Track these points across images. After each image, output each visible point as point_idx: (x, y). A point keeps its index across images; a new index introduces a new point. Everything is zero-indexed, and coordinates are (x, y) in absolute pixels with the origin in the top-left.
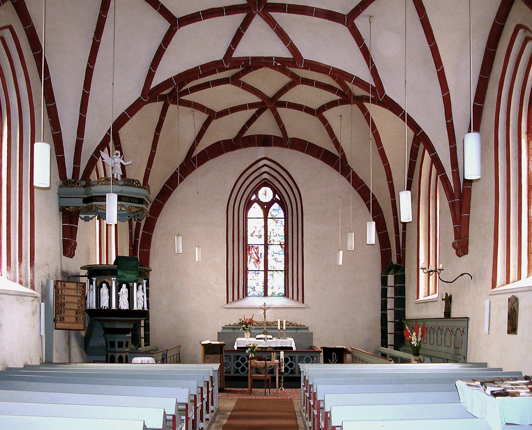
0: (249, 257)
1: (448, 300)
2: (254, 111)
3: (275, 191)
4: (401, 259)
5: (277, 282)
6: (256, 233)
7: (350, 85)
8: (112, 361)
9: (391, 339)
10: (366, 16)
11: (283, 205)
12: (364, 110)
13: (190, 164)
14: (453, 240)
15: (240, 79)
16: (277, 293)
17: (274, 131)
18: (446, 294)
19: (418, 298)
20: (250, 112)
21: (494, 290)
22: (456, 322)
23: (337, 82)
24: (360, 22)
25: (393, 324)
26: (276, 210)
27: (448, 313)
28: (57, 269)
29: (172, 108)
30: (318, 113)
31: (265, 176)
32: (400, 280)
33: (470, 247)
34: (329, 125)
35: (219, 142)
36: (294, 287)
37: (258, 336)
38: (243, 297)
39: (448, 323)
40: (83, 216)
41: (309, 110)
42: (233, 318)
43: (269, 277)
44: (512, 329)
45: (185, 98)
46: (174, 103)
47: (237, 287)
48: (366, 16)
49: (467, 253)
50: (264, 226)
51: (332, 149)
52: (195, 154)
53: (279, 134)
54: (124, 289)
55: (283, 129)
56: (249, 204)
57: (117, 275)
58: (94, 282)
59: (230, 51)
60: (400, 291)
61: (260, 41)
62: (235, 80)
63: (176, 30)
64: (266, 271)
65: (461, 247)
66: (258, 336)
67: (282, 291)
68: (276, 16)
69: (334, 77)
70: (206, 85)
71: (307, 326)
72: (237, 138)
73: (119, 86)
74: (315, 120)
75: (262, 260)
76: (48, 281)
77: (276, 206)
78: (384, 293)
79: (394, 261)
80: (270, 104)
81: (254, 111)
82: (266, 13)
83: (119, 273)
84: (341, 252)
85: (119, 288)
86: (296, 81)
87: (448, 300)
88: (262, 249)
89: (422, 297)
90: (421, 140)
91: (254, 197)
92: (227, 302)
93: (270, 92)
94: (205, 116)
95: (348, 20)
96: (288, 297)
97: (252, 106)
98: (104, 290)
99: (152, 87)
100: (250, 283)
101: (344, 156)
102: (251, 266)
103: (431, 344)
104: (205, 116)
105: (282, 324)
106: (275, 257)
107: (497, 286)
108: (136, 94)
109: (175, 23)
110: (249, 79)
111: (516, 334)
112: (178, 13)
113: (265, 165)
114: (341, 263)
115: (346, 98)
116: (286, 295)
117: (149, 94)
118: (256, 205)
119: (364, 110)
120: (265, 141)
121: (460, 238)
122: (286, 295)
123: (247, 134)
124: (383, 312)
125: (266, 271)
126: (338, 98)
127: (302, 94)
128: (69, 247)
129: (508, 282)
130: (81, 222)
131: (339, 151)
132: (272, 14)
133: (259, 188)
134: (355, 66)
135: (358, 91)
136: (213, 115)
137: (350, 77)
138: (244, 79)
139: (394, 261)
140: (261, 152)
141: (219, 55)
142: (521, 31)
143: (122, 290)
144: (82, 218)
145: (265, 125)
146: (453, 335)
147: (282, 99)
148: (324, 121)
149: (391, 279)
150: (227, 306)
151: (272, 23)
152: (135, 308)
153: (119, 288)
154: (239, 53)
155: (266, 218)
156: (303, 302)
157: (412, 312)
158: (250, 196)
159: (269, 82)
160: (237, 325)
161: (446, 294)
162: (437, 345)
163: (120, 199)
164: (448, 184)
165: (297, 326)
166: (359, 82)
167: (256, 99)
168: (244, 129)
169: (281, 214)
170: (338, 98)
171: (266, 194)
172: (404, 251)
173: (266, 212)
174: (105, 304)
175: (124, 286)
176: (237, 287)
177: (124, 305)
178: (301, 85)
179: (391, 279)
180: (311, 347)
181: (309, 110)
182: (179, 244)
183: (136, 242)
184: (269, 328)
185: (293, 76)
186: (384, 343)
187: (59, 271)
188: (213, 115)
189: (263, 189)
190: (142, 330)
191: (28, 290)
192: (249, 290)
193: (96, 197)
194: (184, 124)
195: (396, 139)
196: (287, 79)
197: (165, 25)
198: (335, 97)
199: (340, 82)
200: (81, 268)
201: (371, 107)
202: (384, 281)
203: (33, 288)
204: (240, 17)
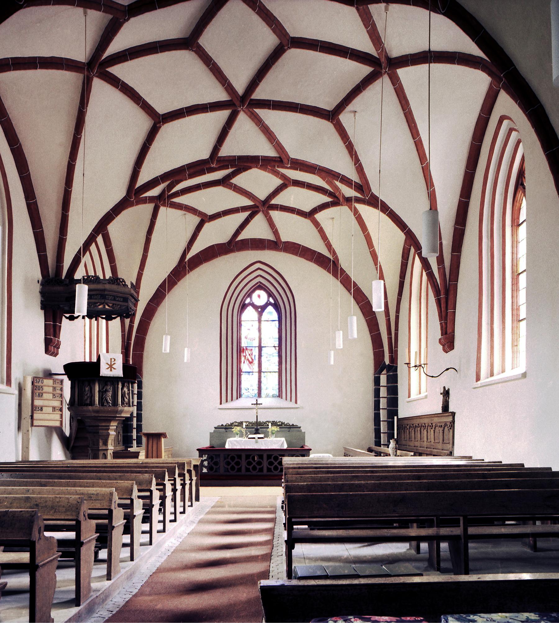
0: (243, 359)
3: (270, 294)
4: (394, 358)
5: (271, 383)
10: (351, 112)
11: (276, 306)
13: (184, 267)
14: (440, 337)
15: (231, 181)
16: (271, 394)
17: (268, 235)
19: (409, 397)
20: (244, 215)
21: (479, 382)
22: (443, 418)
24: (344, 118)
25: (386, 423)
26: (271, 313)
29: (163, 210)
30: (310, 215)
31: (259, 279)
32: (393, 380)
33: (457, 343)
34: (321, 228)
35: (213, 245)
36: (287, 386)
38: (237, 399)
40: (68, 315)
41: (300, 213)
42: (226, 418)
43: (263, 379)
45: (176, 200)
46: (164, 205)
47: (230, 386)
48: (351, 112)
49: (453, 349)
50: (259, 329)
51: (324, 251)
52: (189, 256)
53: (271, 237)
55: (276, 233)
56: (243, 307)
60: (393, 391)
61: (245, 139)
62: (224, 182)
63: (160, 127)
65: (448, 341)
67: (276, 392)
68: (261, 112)
71: (299, 426)
73: (100, 182)
74: (306, 223)
75: (256, 362)
76: (24, 378)
77: (270, 309)
79: (387, 361)
80: (262, 206)
81: (246, 214)
82: (251, 110)
86: (287, 183)
88: (256, 352)
89: (414, 396)
90: (411, 240)
91: (248, 301)
92: (221, 404)
93: (262, 196)
94: (196, 220)
95: (331, 116)
96: (282, 398)
97: (244, 209)
99: (137, 186)
101: (337, 259)
102: (245, 367)
106: (268, 359)
107: (481, 378)
108: (119, 194)
109: (159, 120)
110: (240, 180)
112: (162, 109)
113: (259, 269)
114: (332, 362)
115: (336, 200)
116: (280, 396)
120: (258, 244)
121: (446, 333)
122: (280, 396)
123: (240, 238)
124: (376, 412)
125: (260, 372)
127: (292, 197)
128: (51, 345)
129: (492, 375)
131: (330, 251)
132: (257, 111)
134: (343, 165)
135: (348, 192)
136: (205, 219)
138: (235, 181)
139: (387, 361)
141: (205, 155)
142: (505, 122)
145: (258, 229)
147: (273, 202)
148: (317, 224)
150: (221, 406)
155: (260, 321)
156: (296, 402)
157: (405, 410)
158: (243, 300)
160: (229, 425)
164: (435, 280)
165: (289, 425)
167: (249, 203)
168: (238, 232)
169: (275, 316)
172: (396, 351)
173: (260, 314)
176: (230, 386)
178: (293, 187)
181: (300, 213)
183: (129, 344)
185: (283, 177)
188: (205, 219)
189: (258, 292)
190: (135, 431)
192: (243, 391)
194: (174, 227)
195: (388, 240)
196: (278, 182)
198: (326, 199)
201: (362, 208)
202: (377, 381)
204: (224, 114)
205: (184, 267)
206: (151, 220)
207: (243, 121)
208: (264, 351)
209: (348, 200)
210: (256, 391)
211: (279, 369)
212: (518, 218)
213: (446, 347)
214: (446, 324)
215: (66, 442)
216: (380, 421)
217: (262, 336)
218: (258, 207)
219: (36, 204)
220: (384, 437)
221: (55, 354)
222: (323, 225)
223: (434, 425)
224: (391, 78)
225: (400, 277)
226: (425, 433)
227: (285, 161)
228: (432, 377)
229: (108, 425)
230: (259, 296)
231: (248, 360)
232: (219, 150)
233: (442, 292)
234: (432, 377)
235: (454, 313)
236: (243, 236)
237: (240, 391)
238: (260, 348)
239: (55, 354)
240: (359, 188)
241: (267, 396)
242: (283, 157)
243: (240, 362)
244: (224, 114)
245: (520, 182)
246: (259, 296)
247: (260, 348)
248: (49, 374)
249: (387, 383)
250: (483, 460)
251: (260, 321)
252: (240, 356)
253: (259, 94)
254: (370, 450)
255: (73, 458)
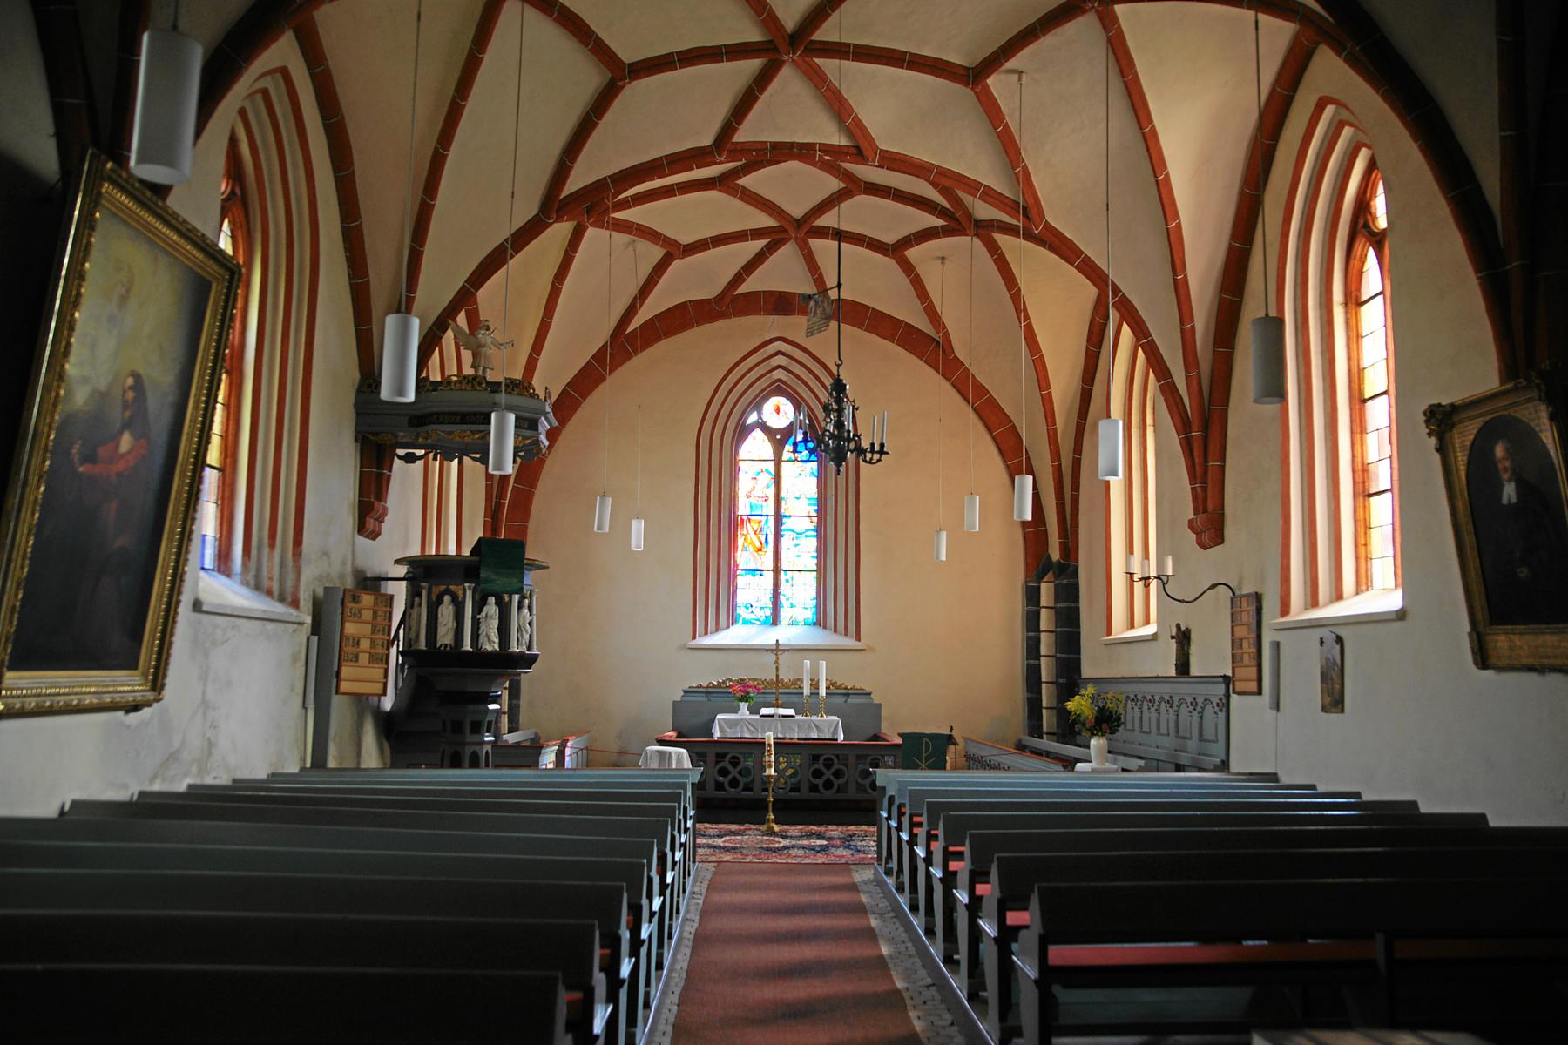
1: (1183, 638)
2: (760, 244)
5: (801, 592)
6: (758, 492)
7: (966, 198)
8: (456, 763)
9: (1048, 720)
12: (993, 248)
13: (623, 344)
16: (800, 619)
18: (1178, 626)
19: (1109, 633)
23: (941, 192)
25: (1053, 687)
27: (1183, 667)
28: (344, 563)
30: (895, 250)
31: (779, 374)
32: (1069, 594)
33: (1229, 531)
34: (917, 276)
37: (764, 711)
39: (1185, 689)
40: (401, 452)
44: (1334, 701)
52: (635, 324)
54: (491, 608)
56: (742, 432)
57: (478, 576)
58: (424, 593)
59: (728, 129)
60: (1069, 618)
61: (791, 111)
62: (723, 183)
64: (777, 570)
66: (764, 711)
67: (810, 615)
68: (827, 65)
69: (934, 185)
70: (668, 192)
71: (868, 690)
72: (720, 298)
75: (770, 548)
78: (1032, 621)
79: (1055, 554)
81: (760, 244)
83: (483, 575)
84: (944, 535)
85: (479, 605)
86: (855, 187)
87: (1183, 638)
89: (1119, 631)
91: (752, 418)
93: (797, 211)
95: (973, 76)
97: (757, 234)
98: (446, 611)
99: (565, 193)
100: (742, 597)
102: (744, 558)
103: (1142, 732)
104: (657, 253)
105: (815, 685)
109: (620, 74)
111: (1324, 709)
112: (628, 56)
114: (943, 557)
115: (957, 222)
117: (553, 206)
118: (758, 433)
119: (993, 248)
120: (782, 303)
121: (1205, 511)
123: (743, 289)
125: (777, 570)
126: (940, 222)
127: (858, 214)
130: (398, 464)
133: (766, 398)
134: (974, 160)
135: (984, 211)
136: (674, 251)
137: (972, 186)
138: (745, 181)
139: (1055, 554)
140: (773, 325)
142: (1329, 110)
143: (485, 609)
144: (400, 458)
145: (783, 272)
146: (1195, 714)
148: (908, 268)
149: (1046, 591)
151: (818, 79)
152: (514, 648)
153: (479, 605)
154: (742, 135)
155: (778, 462)
156: (858, 639)
159: (795, 187)
161: (1178, 626)
162: (1159, 734)
163: (517, 418)
166: (989, 195)
167: (767, 221)
168: (738, 279)
170: (940, 222)
171: (778, 412)
173: (778, 447)
174: (445, 637)
175: (492, 600)
177: (491, 644)
179: (1046, 591)
180: (876, 737)
182: (604, 514)
183: (499, 505)
184: (781, 692)
185: (847, 176)
186: (1035, 729)
187: (349, 569)
188: (674, 251)
189: (775, 401)
191: (278, 609)
193: (438, 414)
194: (606, 266)
195: (1058, 304)
196: (834, 184)
197: (588, 78)
199: (944, 191)
200: (397, 562)
202: (1032, 596)
203: (295, 604)
205: (623, 344)
206: (566, 253)
207: (788, 81)
208: (788, 524)
209: (984, 230)
210: (768, 612)
211: (819, 565)
212: (1359, 289)
213: (1206, 537)
214: (1205, 489)
215: (388, 726)
216: (1040, 682)
217: (783, 494)
218: (786, 231)
219: (359, 229)
220: (1049, 718)
221: (374, 535)
222: (919, 270)
223: (1176, 699)
224: (1101, 19)
225: (1084, 380)
226: (1154, 715)
227: (868, 153)
228: (1182, 601)
229: (472, 687)
230: (778, 411)
231: (752, 543)
232: (735, 130)
233: (1195, 426)
234: (1182, 601)
235: (1222, 469)
236: (750, 285)
237: (734, 609)
238: (779, 518)
239: (374, 535)
240: (1010, 206)
241: (793, 623)
242: (864, 146)
243: (735, 548)
244: (751, 66)
245: (1361, 222)
246: (778, 411)
247: (779, 518)
248: (370, 583)
249: (1056, 601)
250: (1313, 787)
251: (778, 462)
252: (736, 536)
253: (827, 32)
254: (1021, 747)
255: (394, 765)
